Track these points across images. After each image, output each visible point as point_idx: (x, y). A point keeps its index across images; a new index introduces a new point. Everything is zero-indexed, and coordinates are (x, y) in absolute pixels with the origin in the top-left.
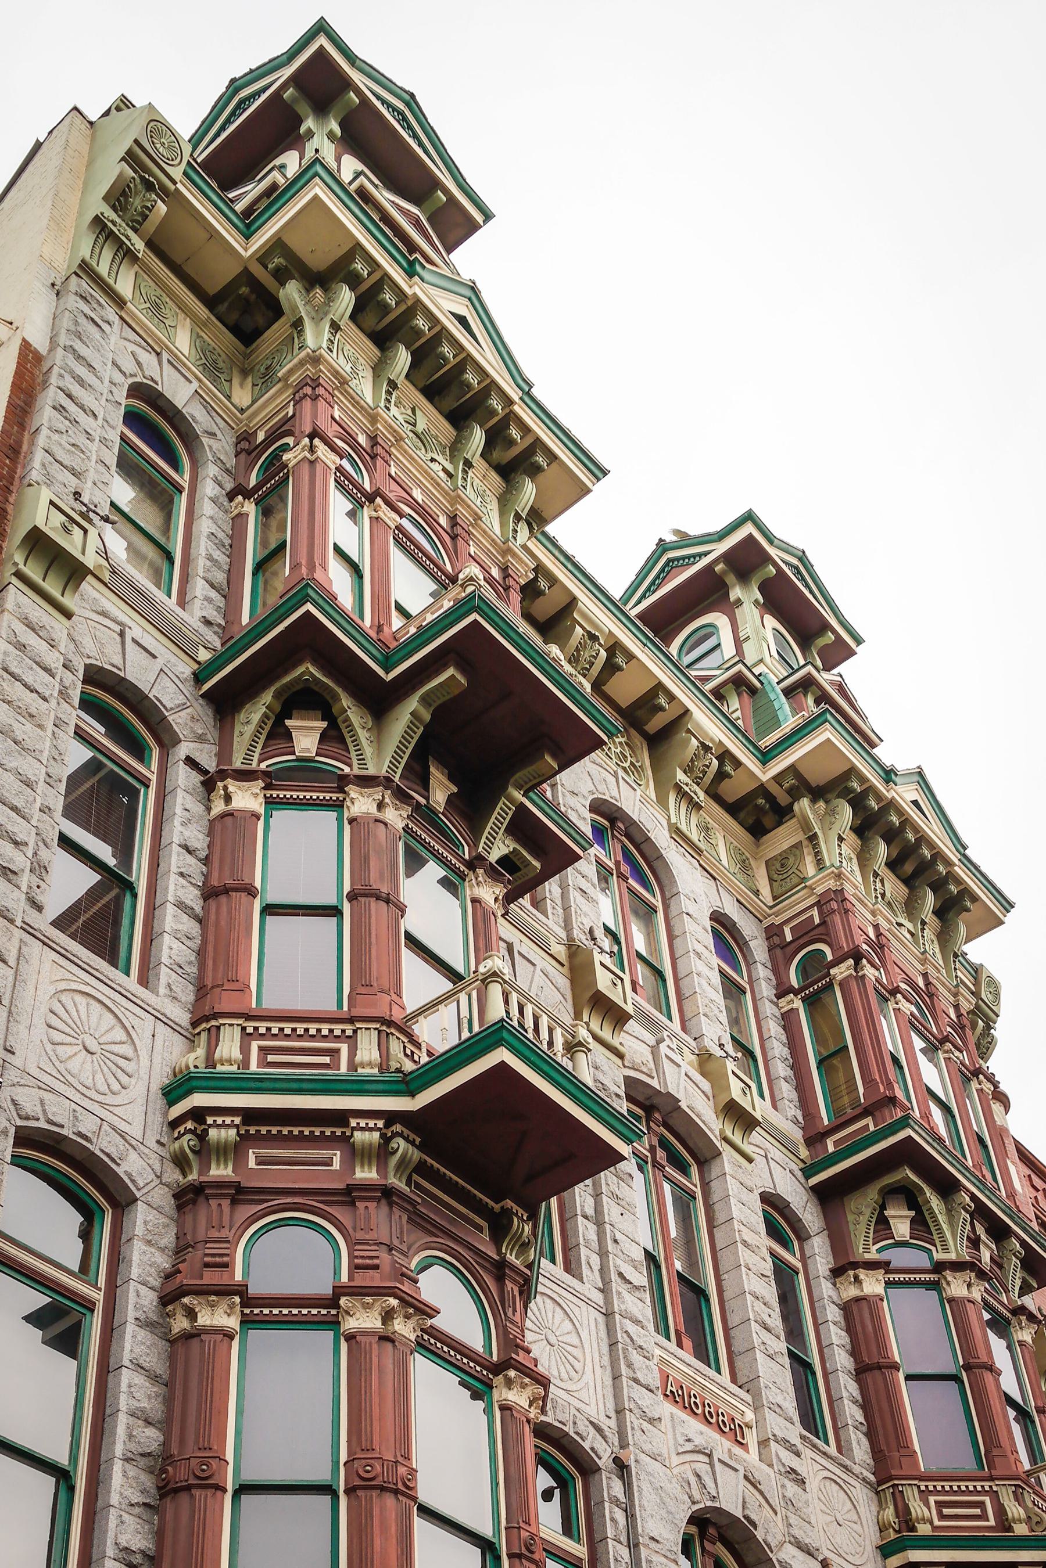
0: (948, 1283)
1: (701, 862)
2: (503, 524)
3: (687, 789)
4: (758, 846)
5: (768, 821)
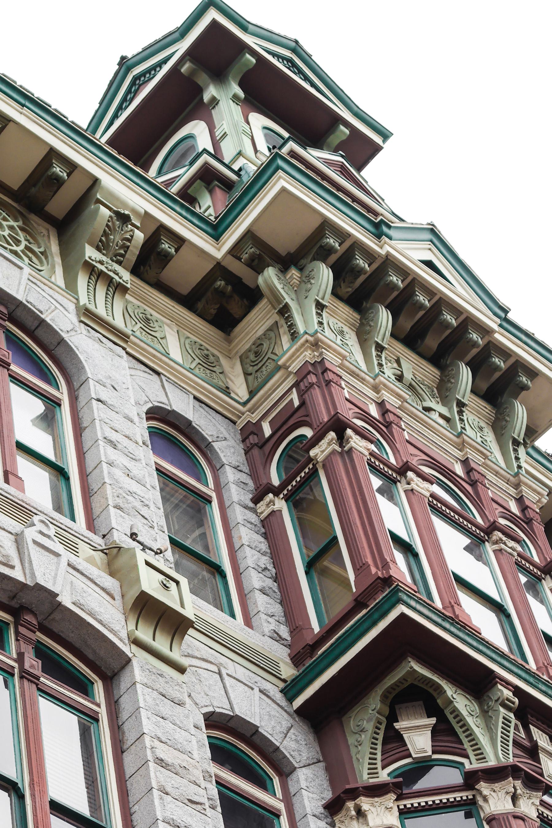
0: (485, 799)
1: (128, 350)
2: (505, 454)
3: (102, 268)
4: (230, 342)
5: (235, 308)
